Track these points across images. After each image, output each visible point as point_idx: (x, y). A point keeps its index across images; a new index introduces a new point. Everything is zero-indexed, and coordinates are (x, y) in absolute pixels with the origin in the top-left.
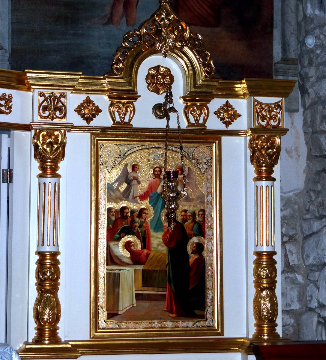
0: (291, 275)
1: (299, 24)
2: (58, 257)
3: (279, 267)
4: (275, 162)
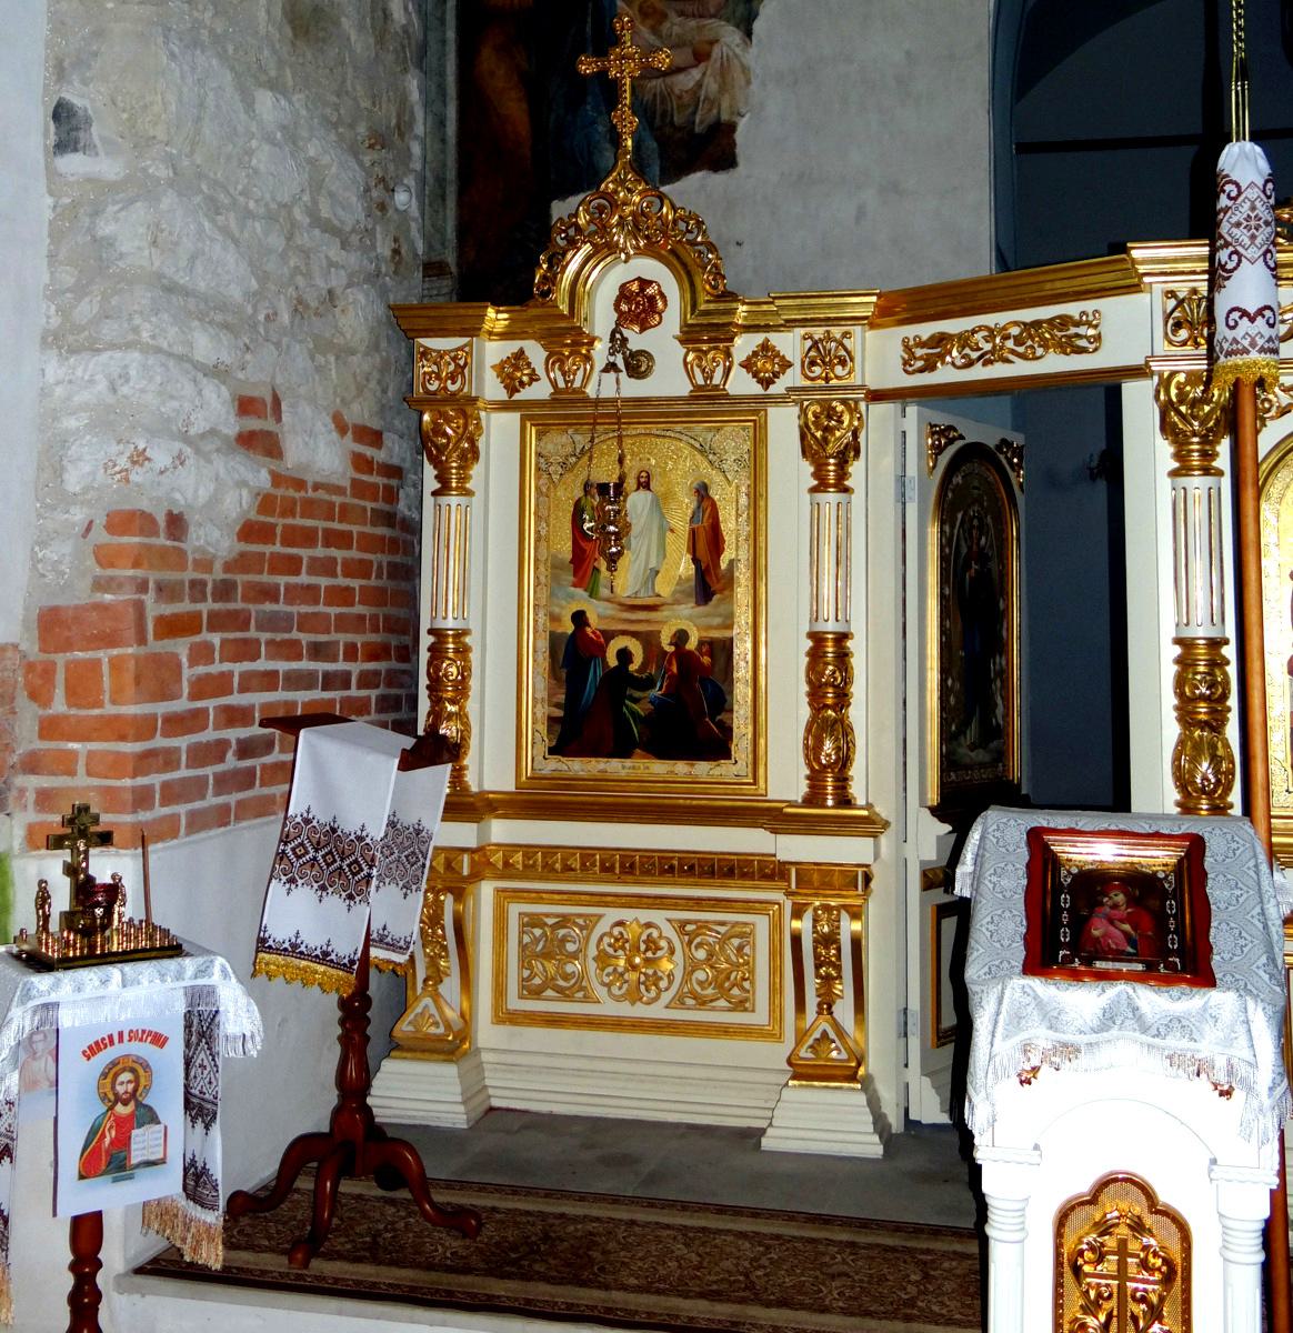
2: (849, 644)
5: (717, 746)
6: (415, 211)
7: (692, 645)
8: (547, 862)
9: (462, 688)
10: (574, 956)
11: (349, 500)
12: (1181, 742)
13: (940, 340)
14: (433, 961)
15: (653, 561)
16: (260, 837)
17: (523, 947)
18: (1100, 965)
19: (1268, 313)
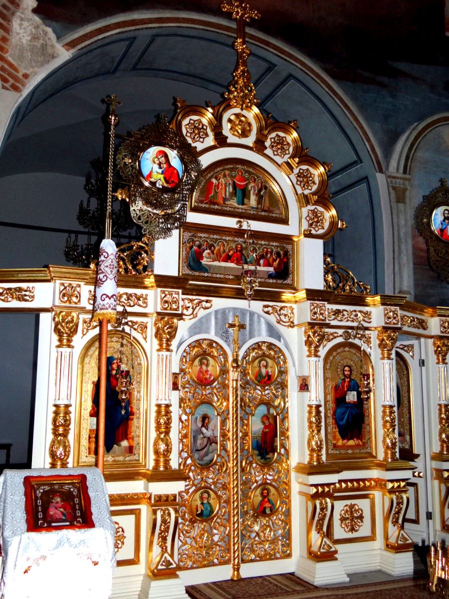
12: (53, 442)
18: (53, 524)
19: (114, 297)
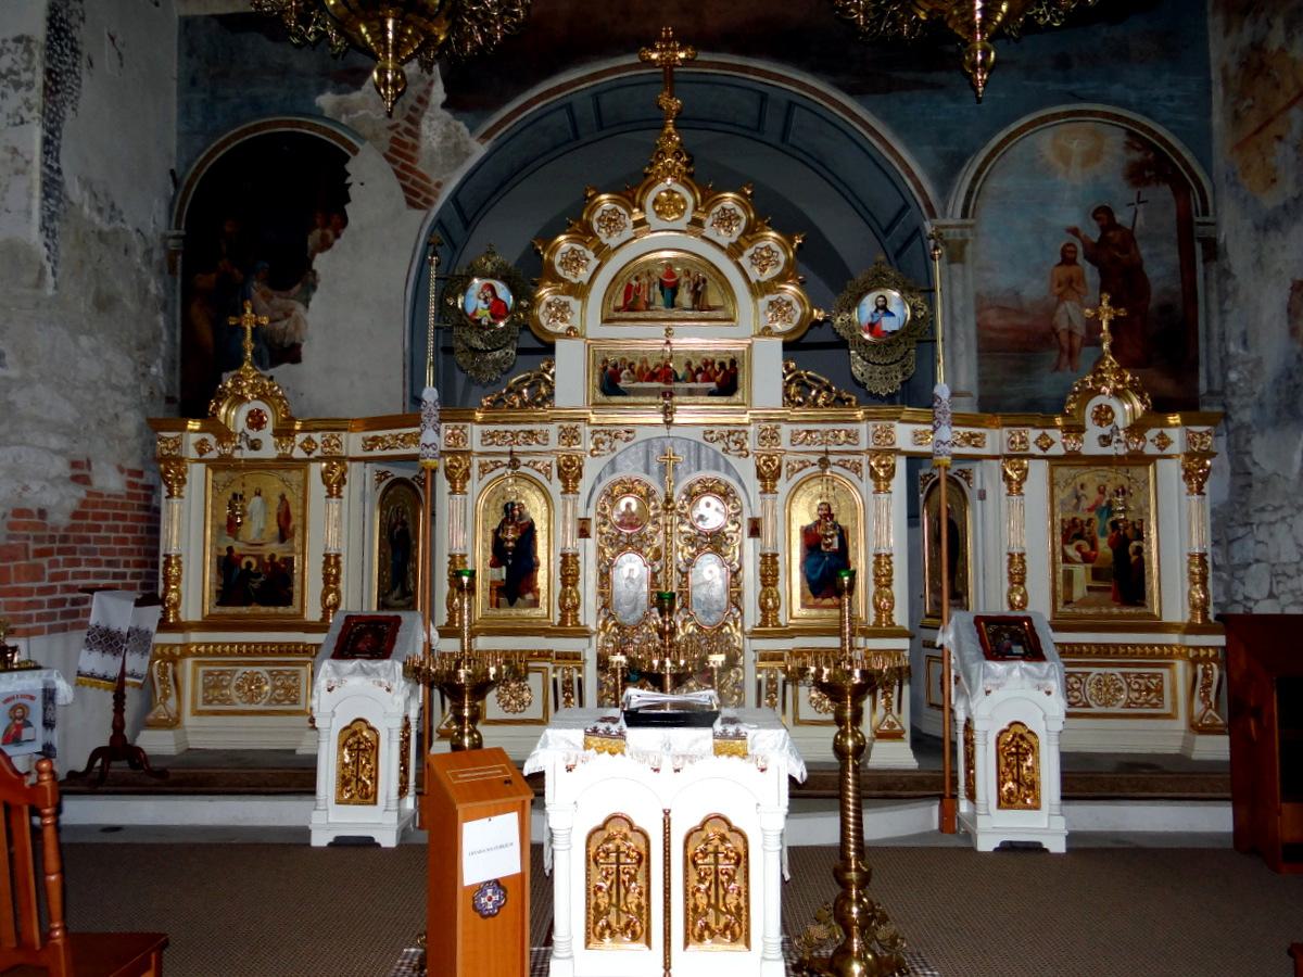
0: (1218, 574)
1: (1222, 360)
3: (1210, 565)
4: (1205, 480)
5: (288, 601)
6: (161, 374)
7: (277, 559)
8: (216, 651)
9: (178, 579)
10: (226, 687)
11: (125, 500)
13: (374, 439)
14: (164, 691)
15: (259, 523)
16: (78, 637)
17: (204, 684)
